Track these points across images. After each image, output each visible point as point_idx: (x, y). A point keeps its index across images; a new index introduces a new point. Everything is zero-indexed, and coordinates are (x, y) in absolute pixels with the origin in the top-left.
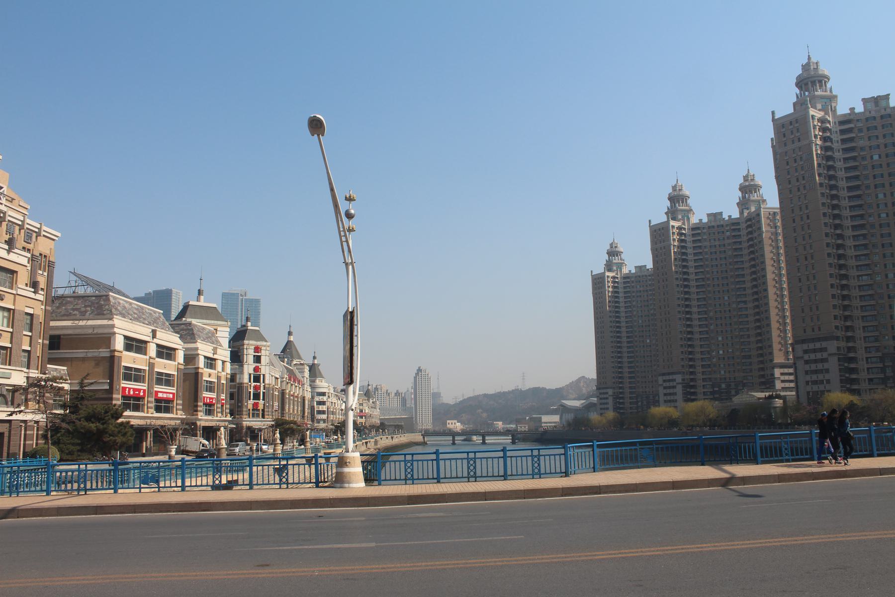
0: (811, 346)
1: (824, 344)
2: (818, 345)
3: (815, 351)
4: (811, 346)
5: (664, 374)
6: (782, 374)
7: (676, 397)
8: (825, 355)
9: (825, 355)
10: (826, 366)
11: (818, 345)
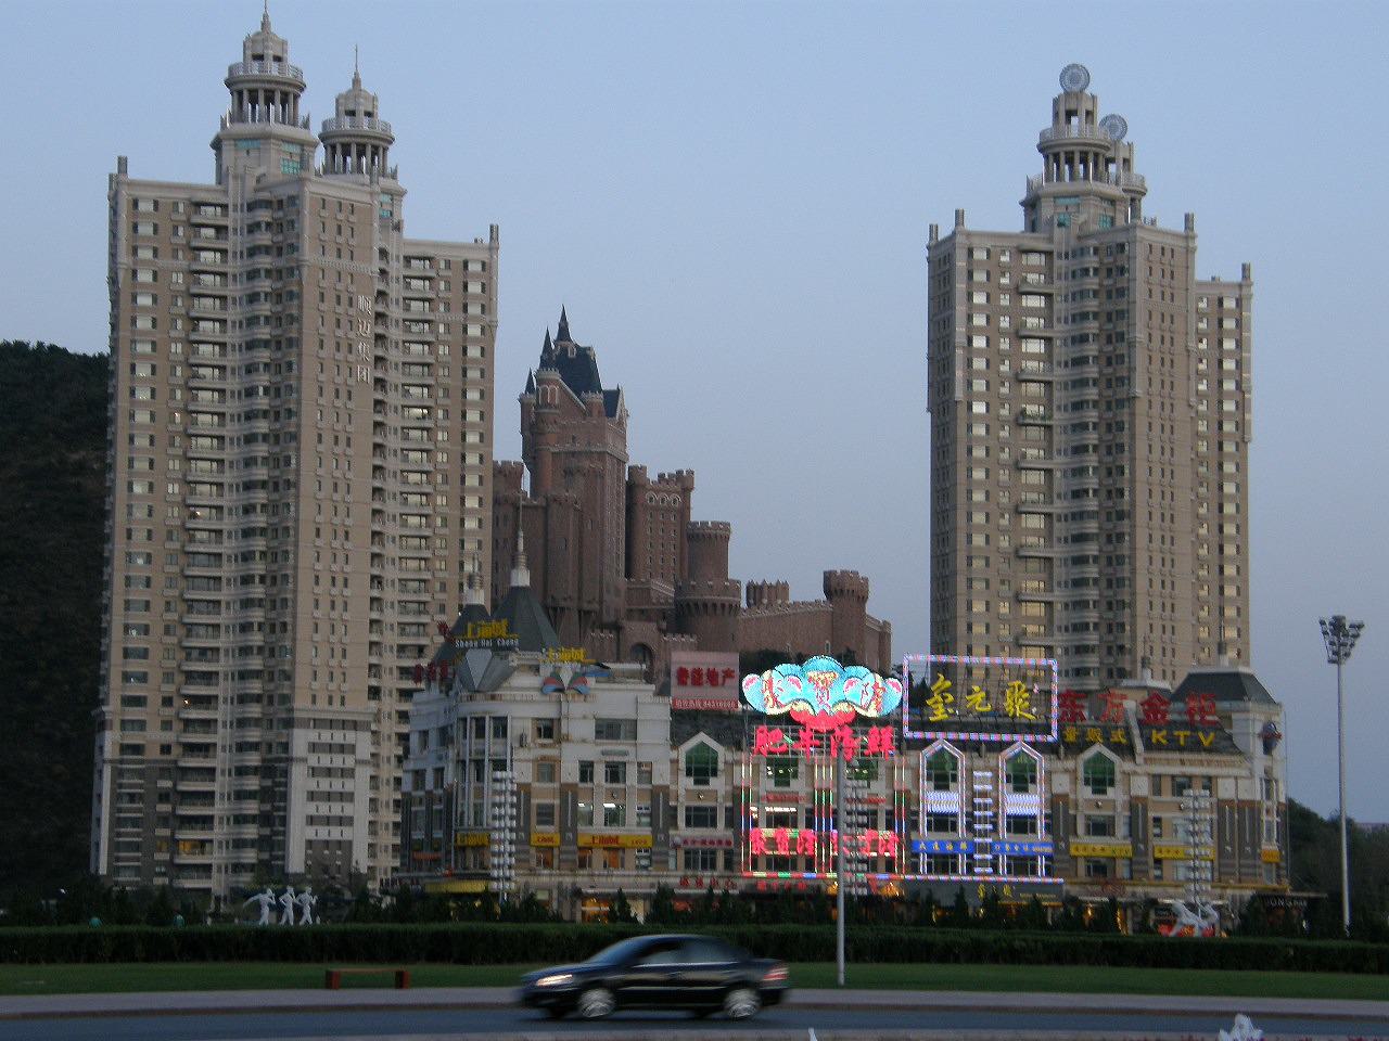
0: (326, 736)
1: (351, 737)
2: (338, 737)
3: (330, 748)
4: (326, 736)
5: (318, 723)
6: (314, 747)
7: (349, 809)
8: (350, 761)
9: (350, 761)
10: (349, 785)
11: (338, 737)
